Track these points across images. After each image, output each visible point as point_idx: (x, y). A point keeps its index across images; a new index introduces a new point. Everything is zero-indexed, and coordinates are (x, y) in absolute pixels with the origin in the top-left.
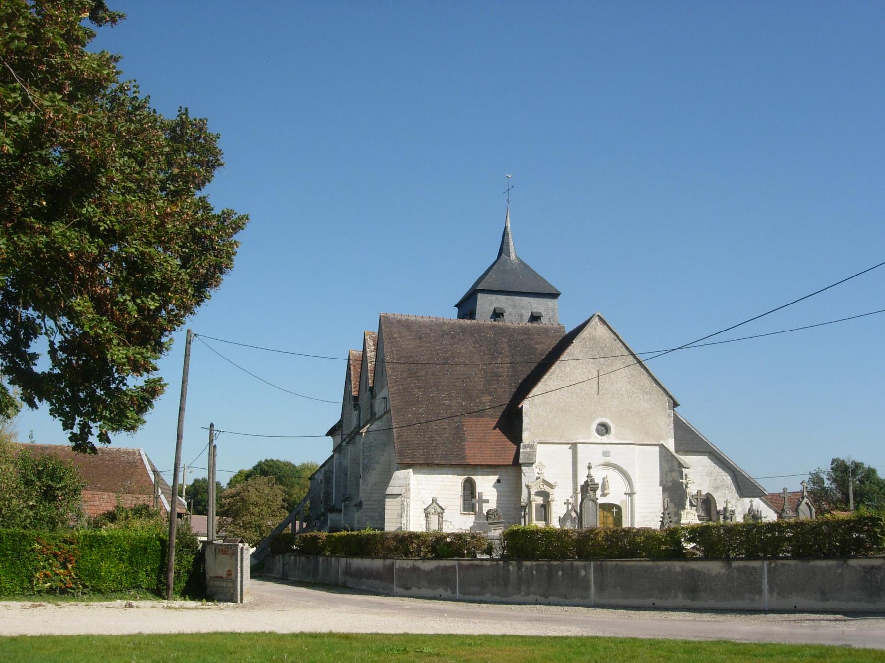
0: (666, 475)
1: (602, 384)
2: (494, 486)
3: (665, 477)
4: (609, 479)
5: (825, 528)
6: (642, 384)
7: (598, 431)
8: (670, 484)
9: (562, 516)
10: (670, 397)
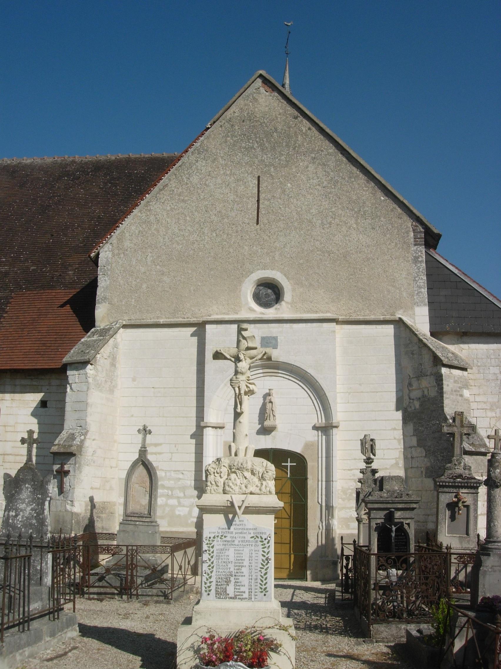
0: (410, 384)
1: (267, 203)
2: (34, 414)
3: (406, 391)
4: (275, 398)
5: (412, 598)
6: (354, 198)
7: (258, 298)
8: (417, 404)
9: (13, 473)
10: (418, 219)
